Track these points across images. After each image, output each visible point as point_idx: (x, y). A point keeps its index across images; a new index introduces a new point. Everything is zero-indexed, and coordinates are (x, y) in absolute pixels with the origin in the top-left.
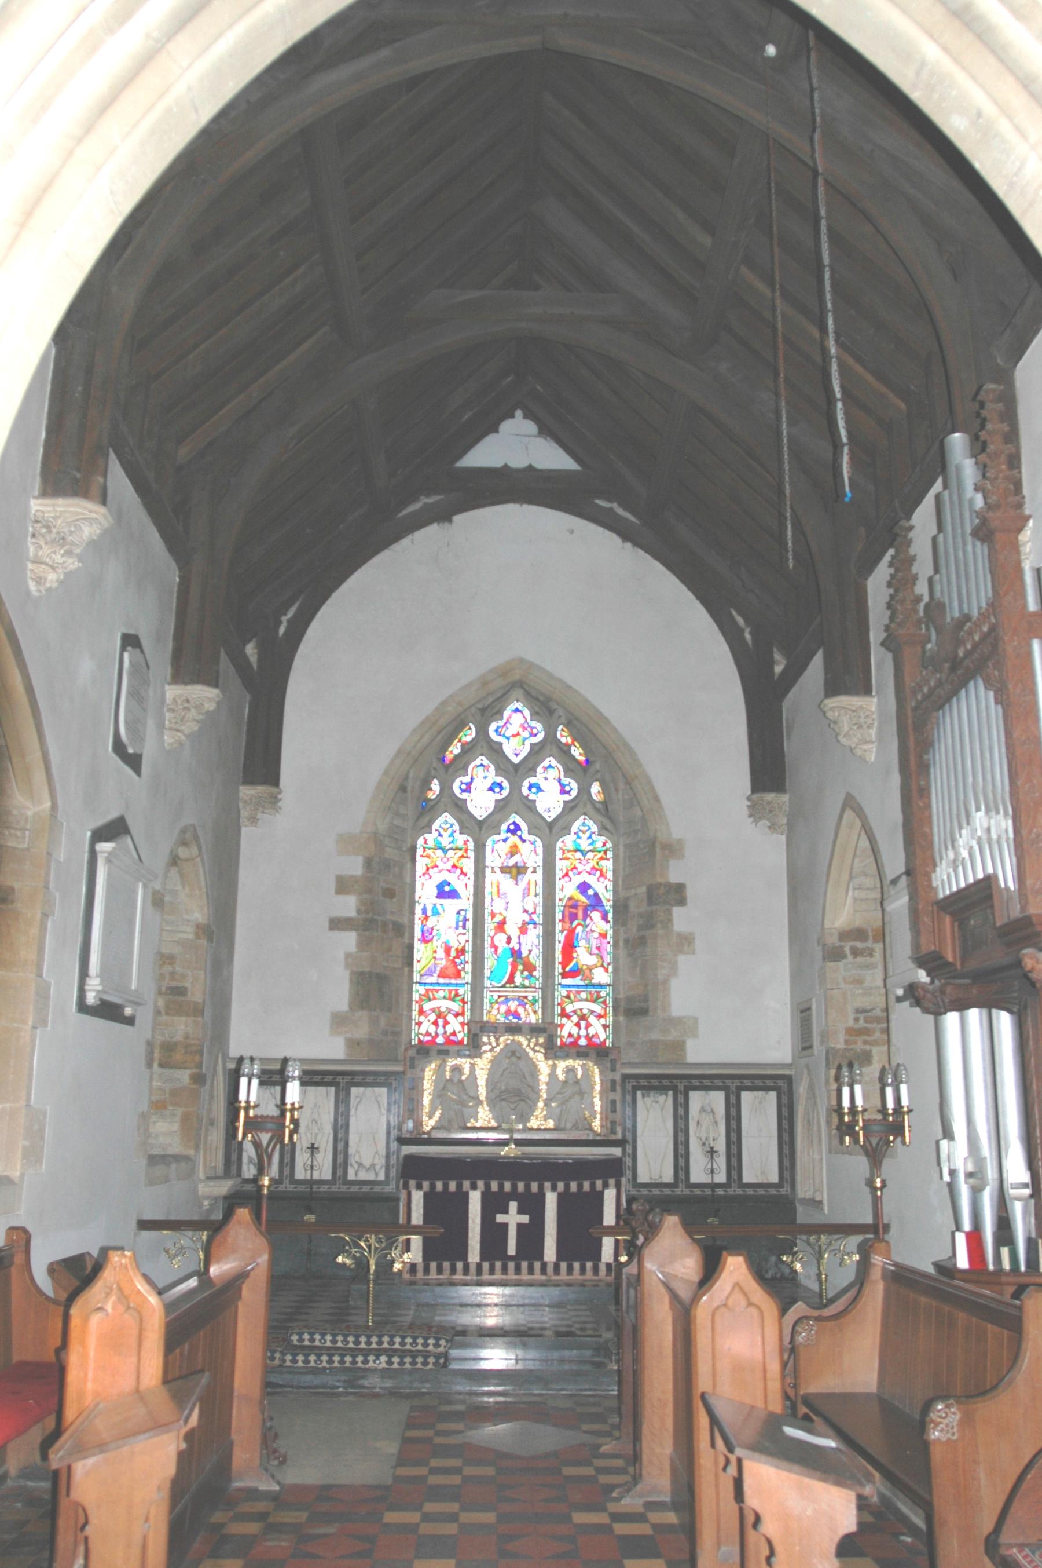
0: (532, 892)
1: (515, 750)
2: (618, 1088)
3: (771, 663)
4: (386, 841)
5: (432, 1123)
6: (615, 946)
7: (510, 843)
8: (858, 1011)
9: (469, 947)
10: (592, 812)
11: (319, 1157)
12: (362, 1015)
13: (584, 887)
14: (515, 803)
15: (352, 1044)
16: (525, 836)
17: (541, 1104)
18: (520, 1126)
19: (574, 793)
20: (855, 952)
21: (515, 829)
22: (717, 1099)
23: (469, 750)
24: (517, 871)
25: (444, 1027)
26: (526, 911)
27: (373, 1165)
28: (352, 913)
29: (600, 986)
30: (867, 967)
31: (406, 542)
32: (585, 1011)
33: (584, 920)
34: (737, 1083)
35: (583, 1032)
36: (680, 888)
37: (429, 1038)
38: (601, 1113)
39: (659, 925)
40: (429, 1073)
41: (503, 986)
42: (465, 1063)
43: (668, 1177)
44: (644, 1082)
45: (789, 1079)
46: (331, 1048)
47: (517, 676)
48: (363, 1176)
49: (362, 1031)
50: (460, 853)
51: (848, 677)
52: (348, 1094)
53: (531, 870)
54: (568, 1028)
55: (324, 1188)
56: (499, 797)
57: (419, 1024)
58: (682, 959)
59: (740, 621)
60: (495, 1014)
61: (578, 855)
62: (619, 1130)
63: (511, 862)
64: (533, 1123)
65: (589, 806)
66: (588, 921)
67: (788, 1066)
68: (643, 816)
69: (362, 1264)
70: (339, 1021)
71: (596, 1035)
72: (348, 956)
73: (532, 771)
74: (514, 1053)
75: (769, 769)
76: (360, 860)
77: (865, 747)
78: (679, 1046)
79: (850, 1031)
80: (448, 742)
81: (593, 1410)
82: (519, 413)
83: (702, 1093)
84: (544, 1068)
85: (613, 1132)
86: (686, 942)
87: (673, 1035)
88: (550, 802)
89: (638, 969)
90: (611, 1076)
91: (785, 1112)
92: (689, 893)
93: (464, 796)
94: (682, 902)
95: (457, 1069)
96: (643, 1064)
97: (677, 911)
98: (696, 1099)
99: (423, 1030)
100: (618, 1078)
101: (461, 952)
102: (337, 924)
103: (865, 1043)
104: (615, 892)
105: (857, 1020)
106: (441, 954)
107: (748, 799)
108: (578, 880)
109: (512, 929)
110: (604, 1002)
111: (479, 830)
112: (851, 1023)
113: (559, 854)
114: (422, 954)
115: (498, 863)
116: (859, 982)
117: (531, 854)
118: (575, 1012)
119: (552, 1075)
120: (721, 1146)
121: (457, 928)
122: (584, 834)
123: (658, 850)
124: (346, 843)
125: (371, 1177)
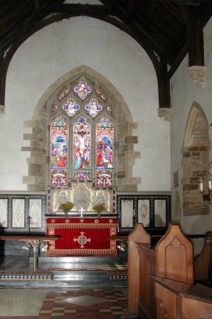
0: (88, 140)
2: (116, 199)
3: (167, 68)
5: (56, 210)
6: (115, 156)
7: (80, 125)
8: (194, 172)
12: (33, 177)
13: (105, 138)
17: (91, 204)
20: (194, 154)
21: (82, 121)
22: (147, 202)
26: (86, 146)
27: (37, 223)
28: (29, 146)
30: (198, 159)
31: (46, 28)
33: (105, 148)
35: (104, 183)
36: (136, 138)
39: (129, 149)
41: (79, 169)
42: (66, 192)
44: (124, 197)
45: (170, 196)
46: (23, 188)
49: (33, 182)
51: (196, 60)
52: (29, 201)
57: (52, 181)
58: (136, 160)
59: (156, 54)
61: (103, 129)
62: (116, 211)
63: (81, 131)
64: (88, 210)
66: (106, 149)
67: (170, 192)
68: (124, 116)
73: (88, 102)
75: (165, 100)
77: (201, 83)
78: (135, 186)
79: (191, 179)
81: (109, 292)
84: (92, 194)
85: (114, 212)
86: (138, 154)
87: (133, 183)
88: (93, 112)
90: (114, 195)
91: (168, 206)
92: (139, 139)
93: (66, 110)
94: (136, 142)
95: (64, 194)
97: (135, 145)
101: (65, 158)
102: (24, 149)
103: (197, 182)
105: (194, 175)
106: (58, 159)
108: (102, 136)
110: (111, 174)
112: (192, 176)
113: (97, 128)
116: (195, 163)
117: (87, 128)
118: (102, 177)
119: (95, 195)
121: (64, 151)
122: (104, 122)
123: (129, 125)
124: (27, 124)
125: (37, 227)
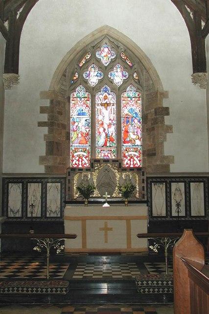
1: (105, 61)
2: (145, 182)
4: (59, 94)
9: (90, 133)
10: (134, 83)
11: (36, 208)
14: (105, 81)
15: (47, 168)
16: (110, 92)
18: (109, 196)
19: (127, 77)
22: (182, 186)
23: (87, 62)
24: (106, 105)
25: (82, 162)
27: (56, 211)
28: (46, 120)
29: (138, 145)
32: (132, 155)
34: (189, 180)
36: (167, 109)
37: (76, 166)
38: (139, 191)
40: (76, 178)
43: (164, 214)
44: (154, 180)
47: (105, 32)
48: (52, 215)
50: (86, 99)
53: (112, 105)
54: (126, 162)
55: (38, 220)
56: (99, 78)
57: (73, 161)
58: (168, 135)
60: (100, 156)
61: (129, 99)
62: (146, 197)
64: (114, 195)
65: (133, 81)
69: (44, 250)
70: (42, 159)
71: (137, 164)
72: (45, 135)
74: (107, 170)
76: (49, 101)
78: (167, 166)
80: (80, 61)
82: (106, 231)
83: (176, 183)
84: (118, 175)
85: (144, 198)
86: (169, 129)
87: (165, 162)
89: (152, 140)
90: (142, 177)
92: (170, 110)
93: (87, 78)
94: (168, 114)
96: (153, 174)
98: (174, 186)
99: (74, 163)
100: (145, 179)
102: (41, 124)
104: (143, 112)
107: (192, 76)
108: (129, 108)
109: (106, 126)
111: (93, 91)
114: (73, 136)
115: (100, 102)
119: (121, 177)
120: (183, 203)
122: (131, 92)
